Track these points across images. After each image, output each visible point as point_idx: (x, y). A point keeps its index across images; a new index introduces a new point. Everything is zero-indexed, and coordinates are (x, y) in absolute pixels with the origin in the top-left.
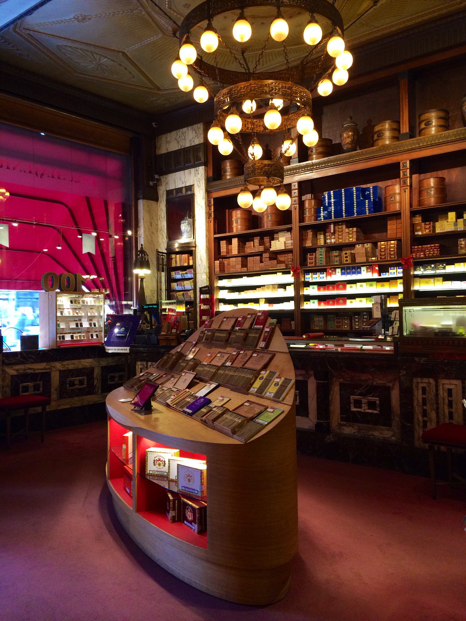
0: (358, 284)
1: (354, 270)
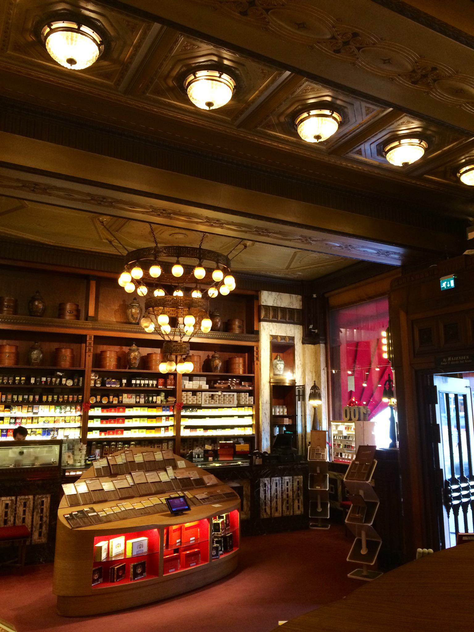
0: (134, 419)
1: (168, 409)
